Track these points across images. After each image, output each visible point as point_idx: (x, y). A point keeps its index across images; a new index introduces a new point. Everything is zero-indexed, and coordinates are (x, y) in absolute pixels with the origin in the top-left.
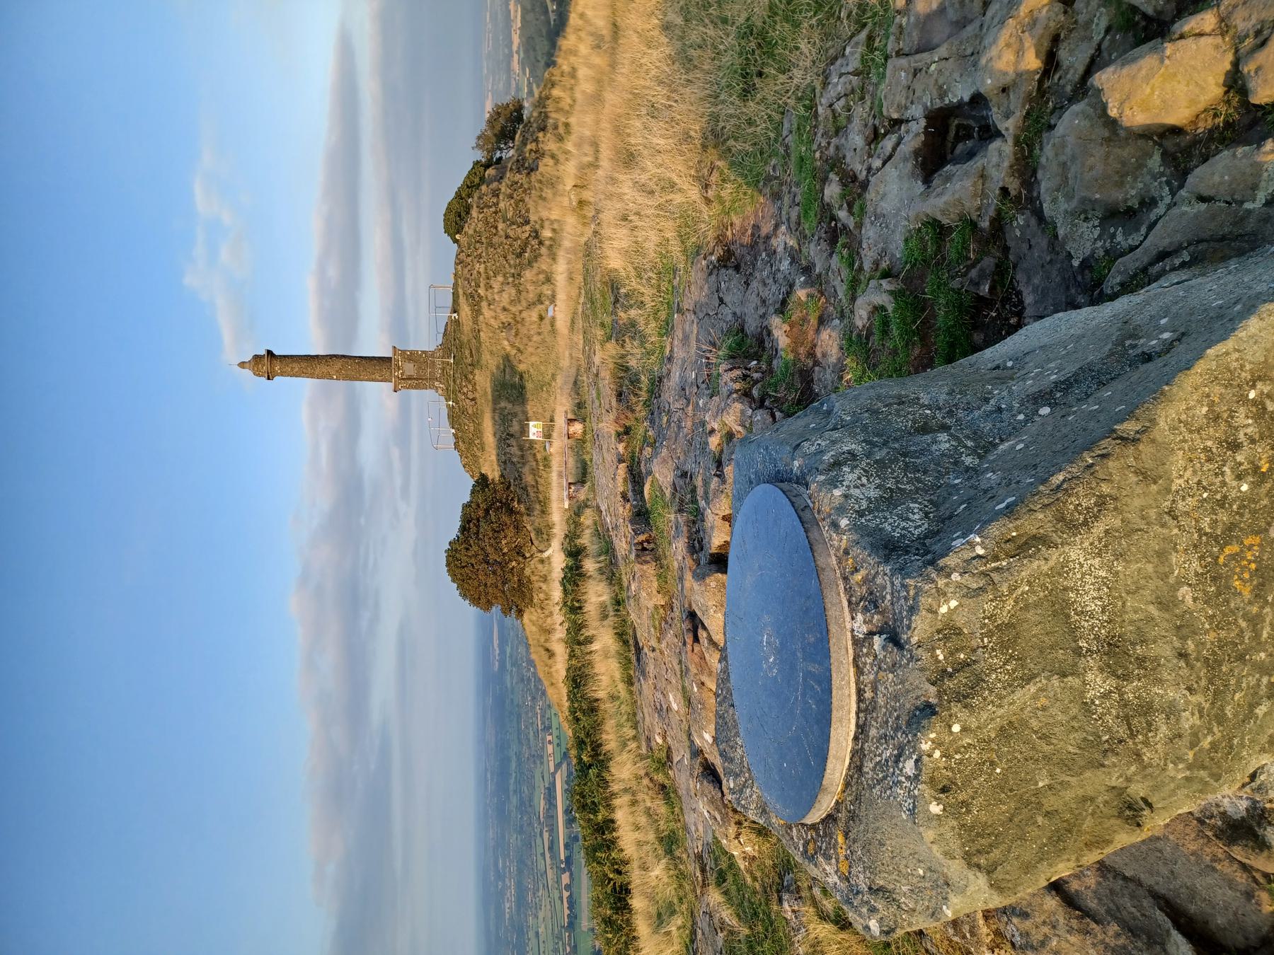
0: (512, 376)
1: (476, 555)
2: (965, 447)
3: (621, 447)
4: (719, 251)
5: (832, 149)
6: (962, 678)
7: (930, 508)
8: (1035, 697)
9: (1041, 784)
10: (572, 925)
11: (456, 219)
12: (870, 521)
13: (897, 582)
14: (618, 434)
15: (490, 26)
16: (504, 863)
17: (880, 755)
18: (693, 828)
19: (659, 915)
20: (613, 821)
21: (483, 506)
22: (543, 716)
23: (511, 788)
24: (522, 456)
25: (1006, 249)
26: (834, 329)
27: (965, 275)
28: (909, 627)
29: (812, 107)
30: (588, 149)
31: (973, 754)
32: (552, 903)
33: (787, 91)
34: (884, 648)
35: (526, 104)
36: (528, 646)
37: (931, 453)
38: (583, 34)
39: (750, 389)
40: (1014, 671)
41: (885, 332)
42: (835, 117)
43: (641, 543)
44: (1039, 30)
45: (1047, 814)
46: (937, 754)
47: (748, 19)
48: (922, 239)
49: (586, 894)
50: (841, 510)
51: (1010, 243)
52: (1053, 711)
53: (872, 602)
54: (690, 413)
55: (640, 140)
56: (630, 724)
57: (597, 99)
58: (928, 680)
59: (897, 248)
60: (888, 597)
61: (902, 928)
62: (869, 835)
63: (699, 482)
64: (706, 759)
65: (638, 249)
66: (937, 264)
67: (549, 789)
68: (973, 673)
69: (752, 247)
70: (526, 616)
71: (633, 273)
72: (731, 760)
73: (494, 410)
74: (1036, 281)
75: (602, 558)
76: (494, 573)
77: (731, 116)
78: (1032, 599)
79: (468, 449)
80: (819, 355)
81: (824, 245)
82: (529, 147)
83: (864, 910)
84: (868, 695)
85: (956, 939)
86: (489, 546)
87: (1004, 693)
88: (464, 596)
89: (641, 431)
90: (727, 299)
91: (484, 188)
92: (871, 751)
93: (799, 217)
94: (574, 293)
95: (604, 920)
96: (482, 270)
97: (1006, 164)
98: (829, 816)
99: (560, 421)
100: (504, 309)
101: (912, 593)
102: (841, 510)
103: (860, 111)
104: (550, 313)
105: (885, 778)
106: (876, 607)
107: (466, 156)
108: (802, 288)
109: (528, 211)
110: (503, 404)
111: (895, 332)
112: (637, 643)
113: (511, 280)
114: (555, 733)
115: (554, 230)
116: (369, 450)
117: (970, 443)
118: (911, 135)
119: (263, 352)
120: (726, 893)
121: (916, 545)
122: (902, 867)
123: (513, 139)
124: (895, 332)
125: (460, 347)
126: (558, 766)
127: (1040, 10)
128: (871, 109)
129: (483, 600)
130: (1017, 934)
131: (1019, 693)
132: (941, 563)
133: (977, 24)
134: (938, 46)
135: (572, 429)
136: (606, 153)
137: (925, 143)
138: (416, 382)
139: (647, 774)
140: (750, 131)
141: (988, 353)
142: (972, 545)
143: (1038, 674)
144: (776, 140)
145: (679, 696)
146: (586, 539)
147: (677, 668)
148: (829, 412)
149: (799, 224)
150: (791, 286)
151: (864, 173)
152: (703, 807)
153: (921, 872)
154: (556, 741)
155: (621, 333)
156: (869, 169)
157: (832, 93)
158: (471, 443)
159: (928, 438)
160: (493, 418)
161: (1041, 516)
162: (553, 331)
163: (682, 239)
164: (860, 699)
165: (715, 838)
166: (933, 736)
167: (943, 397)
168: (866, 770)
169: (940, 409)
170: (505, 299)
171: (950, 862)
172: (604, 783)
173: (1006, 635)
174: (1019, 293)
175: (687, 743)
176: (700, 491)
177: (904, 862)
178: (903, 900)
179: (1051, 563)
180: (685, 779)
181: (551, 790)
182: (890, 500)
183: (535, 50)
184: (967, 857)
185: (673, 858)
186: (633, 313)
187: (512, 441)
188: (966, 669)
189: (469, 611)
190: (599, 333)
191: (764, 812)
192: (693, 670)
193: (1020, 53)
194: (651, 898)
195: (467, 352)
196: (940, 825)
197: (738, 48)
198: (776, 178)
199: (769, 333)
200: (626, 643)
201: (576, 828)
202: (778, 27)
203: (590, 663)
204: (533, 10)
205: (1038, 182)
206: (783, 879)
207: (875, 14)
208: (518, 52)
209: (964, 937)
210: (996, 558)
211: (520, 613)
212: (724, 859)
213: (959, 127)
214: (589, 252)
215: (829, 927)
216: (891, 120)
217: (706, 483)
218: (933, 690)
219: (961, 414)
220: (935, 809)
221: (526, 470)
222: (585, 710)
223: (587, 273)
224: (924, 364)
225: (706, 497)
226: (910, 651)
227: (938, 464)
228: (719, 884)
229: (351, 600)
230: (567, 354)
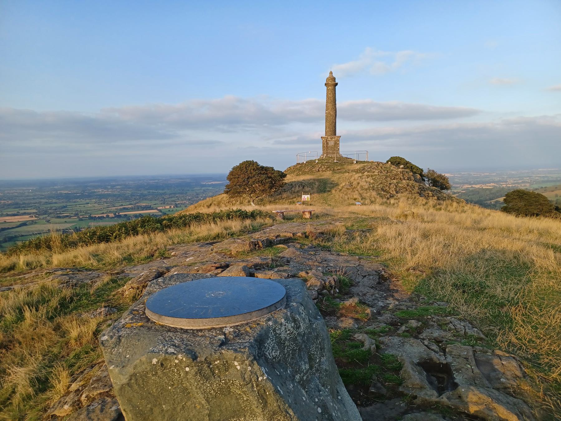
1: (251, 173)
2: (303, 376)
3: (299, 234)
4: (386, 275)
5: (432, 323)
6: (208, 371)
7: (277, 360)
8: (200, 403)
9: (164, 406)
10: (92, 218)
11: (396, 161)
12: (271, 334)
13: (247, 344)
14: (305, 233)
15: (483, 175)
16: (119, 189)
17: (175, 339)
18: (135, 269)
19: (98, 255)
20: (137, 234)
21: (273, 176)
22: (182, 204)
23: (151, 191)
24: (294, 192)
25: (390, 399)
26: (353, 325)
27: (379, 381)
28: (228, 349)
29: (450, 314)
30: (430, 219)
31: (176, 377)
32: (100, 210)
33: (457, 304)
34: (219, 340)
35: (449, 191)
36: (212, 196)
37: (300, 361)
38: (481, 215)
39: (326, 289)
40: (211, 394)
41: (353, 347)
42: (446, 324)
43: (258, 244)
44: (487, 412)
45: (151, 409)
46: (177, 361)
47: (488, 286)
48: (393, 362)
49: (108, 224)
50: (276, 322)
51: (392, 401)
52: (194, 411)
53: (238, 335)
54: (315, 264)
55: (434, 240)
56: (180, 241)
57: (452, 221)
58: (207, 357)
59: (390, 352)
60: (240, 341)
61: (104, 349)
62: (142, 335)
63: (285, 268)
64: (165, 273)
65: (385, 241)
66: (383, 369)
67: (150, 207)
68: (210, 376)
69: (389, 290)
70: (225, 195)
71: (375, 239)
72: (170, 280)
73: (314, 180)
74: (377, 412)
75: (251, 227)
76: (244, 181)
77: (445, 280)
78: (241, 401)
79: (297, 169)
80: (342, 319)
81: (390, 320)
82: (430, 193)
83: (111, 334)
84: (200, 334)
85: (91, 381)
86: (254, 178)
87: (202, 390)
88: (234, 169)
89: (307, 243)
90: (365, 279)
91: (411, 173)
92: (177, 335)
93: (402, 309)
94: (367, 213)
95: (95, 232)
96: (375, 173)
97: (427, 398)
98: (149, 320)
99: (310, 208)
100: (358, 183)
101: (242, 350)
102: (276, 322)
103: (449, 335)
104: (357, 203)
105: (166, 341)
106: (236, 336)
107: (425, 166)
108: (371, 311)
109: (402, 193)
110: (317, 183)
111: (352, 351)
112: (214, 243)
114: (175, 209)
115: (394, 204)
116: (297, 127)
117: (305, 378)
118: (439, 357)
119: (337, 81)
120: (108, 283)
121: (262, 353)
122: (130, 349)
123: (433, 186)
124: (352, 351)
126: (160, 211)
127: (495, 412)
128: (450, 340)
129: (232, 177)
130: (94, 407)
131: (202, 396)
132: (255, 362)
133: (490, 386)
134: (479, 369)
135: (307, 213)
136: (428, 226)
137: (435, 363)
138: (326, 146)
139: (158, 248)
140: (439, 288)
141: (344, 389)
142: (263, 375)
143: (209, 404)
144: (435, 299)
145: (192, 261)
146: (259, 220)
147: (204, 260)
148: (316, 319)
149: (399, 309)
150: (372, 307)
151: (422, 337)
152: (145, 273)
153: (128, 356)
154: (171, 210)
155: (350, 233)
156: (424, 339)
157: (457, 323)
158: (300, 170)
159: (307, 360)
160: (311, 179)
161: (275, 405)
162: (350, 205)
163: (391, 259)
164: (198, 331)
165: (131, 278)
166: (184, 359)
167: (324, 367)
168: (169, 333)
169: (319, 366)
170: (363, 183)
171: (132, 368)
172: (154, 230)
173: (226, 391)
174: (371, 405)
175: (172, 265)
176: (281, 268)
177: (131, 349)
178: (116, 349)
179: (256, 410)
180: (156, 265)
181: (150, 208)
182: (280, 343)
183: (473, 195)
184: (134, 375)
185: (122, 261)
186: (358, 238)
188: (211, 374)
189: (227, 171)
190: (349, 224)
191: (149, 293)
192: (204, 267)
193: (476, 403)
194: (104, 252)
195: (339, 168)
196: (148, 363)
197: (475, 282)
198: (419, 300)
199: (351, 297)
200: (215, 238)
201: (134, 219)
202: (485, 299)
203: (206, 223)
204: (491, 194)
205: (420, 412)
206: (116, 308)
207: (492, 341)
208: (472, 187)
209: (92, 384)
210: (257, 386)
211: (227, 192)
212: (123, 282)
213: (443, 378)
214: (385, 219)
215: (95, 328)
216: (445, 348)
217: (285, 271)
218: (203, 359)
219: (317, 375)
220: (155, 361)
222: (185, 222)
223: (375, 218)
224: (339, 364)
225: (279, 271)
226: (219, 350)
227: (296, 364)
229: (232, 121)
230: (340, 211)
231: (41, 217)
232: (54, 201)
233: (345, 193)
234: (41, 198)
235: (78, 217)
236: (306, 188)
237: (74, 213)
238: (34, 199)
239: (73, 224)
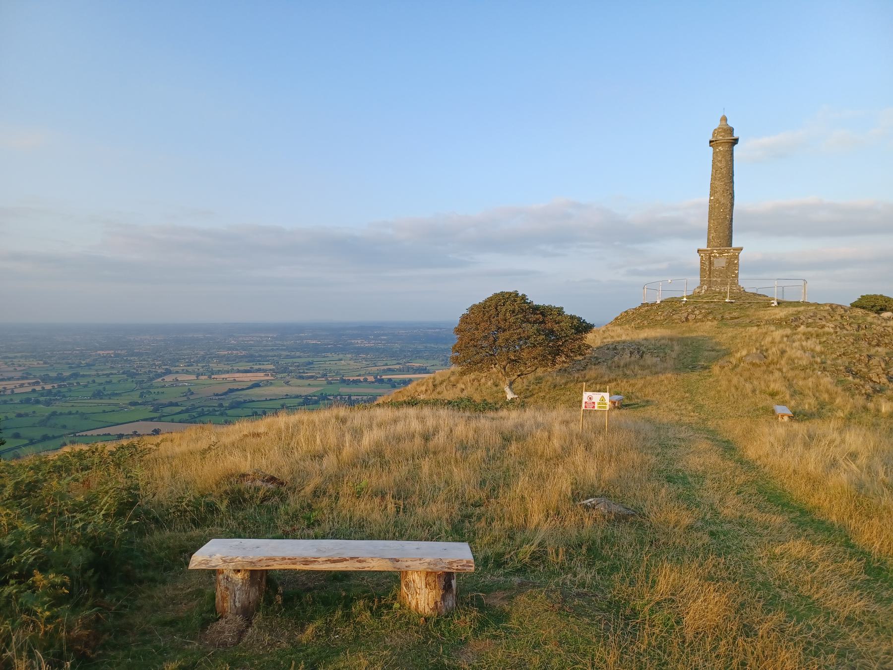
10: (343, 381)
16: (384, 340)
21: (556, 327)
73: (671, 339)
79: (640, 314)
88: (472, 309)
96: (826, 329)
100: (783, 352)
110: (676, 348)
113: (819, 360)
119: (736, 135)
125: (741, 307)
129: (464, 326)
138: (707, 268)
160: (663, 338)
195: (735, 314)
221: (602, 369)
231: (279, 376)
232: (298, 354)
233: (746, 374)
234: (282, 350)
235: (327, 379)
236: (647, 357)
237: (321, 372)
238: (273, 350)
239: (319, 389)
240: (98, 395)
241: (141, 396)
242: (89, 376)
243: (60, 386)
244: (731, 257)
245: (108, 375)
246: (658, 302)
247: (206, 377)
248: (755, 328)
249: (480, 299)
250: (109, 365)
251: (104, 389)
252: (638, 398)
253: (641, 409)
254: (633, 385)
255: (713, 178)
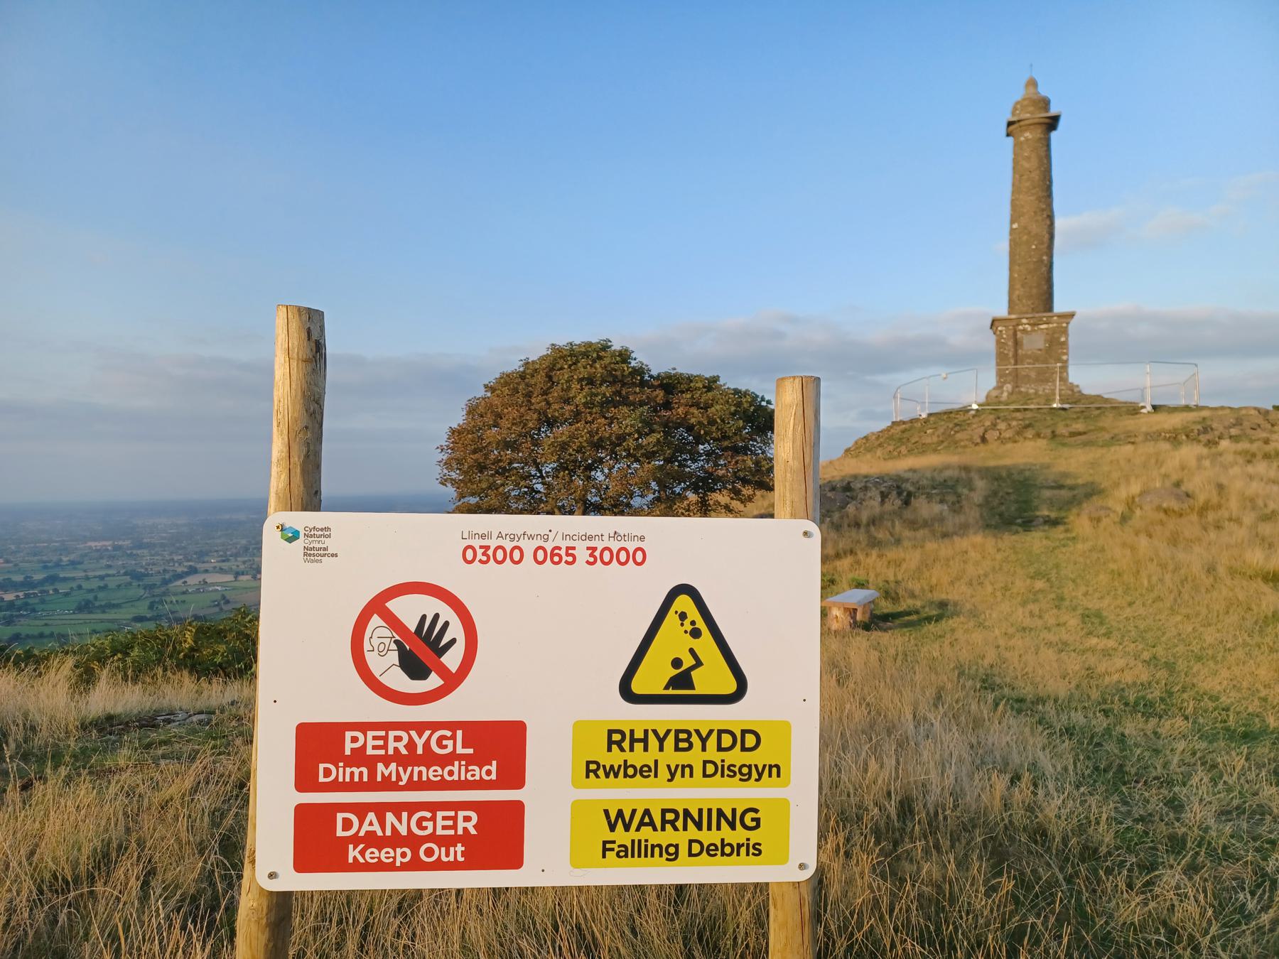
0: (1051, 503)
24: (857, 525)
79: (891, 438)
110: (980, 484)
160: (947, 467)
187: (894, 503)
195: (1079, 426)
228: (1216, 443)
240: (85, 607)
241: (151, 607)
242: (73, 579)
243: (27, 596)
244: (1054, 331)
245: (102, 578)
246: (924, 416)
247: (249, 577)
248: (1130, 448)
249: (514, 365)
250: (104, 562)
251: (96, 598)
252: (913, 596)
253: (931, 627)
254: (898, 564)
255: (1016, 190)
